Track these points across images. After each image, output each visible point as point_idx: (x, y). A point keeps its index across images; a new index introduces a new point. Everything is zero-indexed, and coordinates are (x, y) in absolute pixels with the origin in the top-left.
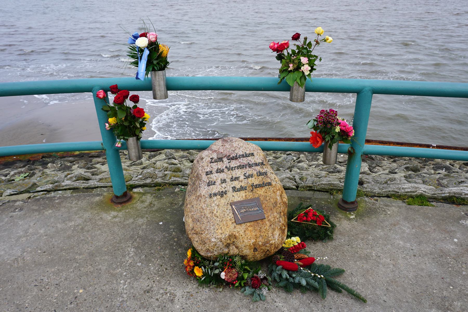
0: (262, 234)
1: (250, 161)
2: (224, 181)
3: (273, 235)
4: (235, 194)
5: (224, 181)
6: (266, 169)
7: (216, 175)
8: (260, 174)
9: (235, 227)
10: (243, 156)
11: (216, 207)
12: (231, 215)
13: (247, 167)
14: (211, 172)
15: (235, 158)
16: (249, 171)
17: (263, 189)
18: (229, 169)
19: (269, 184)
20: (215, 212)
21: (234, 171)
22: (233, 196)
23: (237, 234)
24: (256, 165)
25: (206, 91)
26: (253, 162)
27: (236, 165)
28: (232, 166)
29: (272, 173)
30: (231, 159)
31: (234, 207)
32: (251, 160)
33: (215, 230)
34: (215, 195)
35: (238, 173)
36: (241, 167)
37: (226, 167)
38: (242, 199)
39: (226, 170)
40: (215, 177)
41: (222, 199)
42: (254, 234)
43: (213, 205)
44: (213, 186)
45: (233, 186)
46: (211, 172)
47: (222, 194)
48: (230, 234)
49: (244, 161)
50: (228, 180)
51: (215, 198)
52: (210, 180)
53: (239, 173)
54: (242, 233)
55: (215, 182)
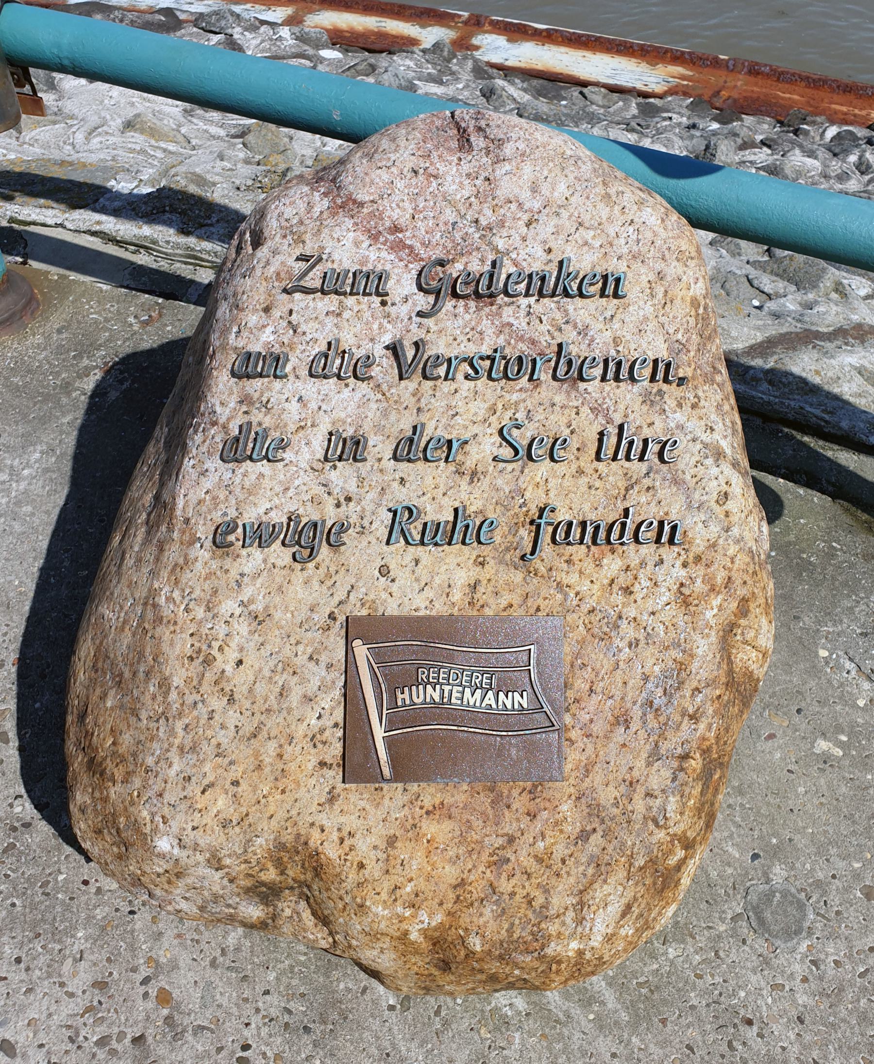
0: (505, 886)
1: (583, 332)
2: (349, 448)
3: (581, 903)
4: (399, 556)
5: (349, 448)
6: (679, 417)
7: (311, 388)
8: (619, 445)
9: (332, 798)
10: (539, 286)
11: (242, 628)
12: (331, 703)
13: (544, 375)
14: (278, 360)
15: (483, 291)
16: (547, 408)
17: (612, 565)
18: (413, 362)
19: (667, 534)
20: (225, 662)
21: (446, 387)
22: (384, 570)
23: (332, 852)
24: (617, 370)
25: (327, 139)
26: (601, 344)
27: (470, 349)
28: (438, 347)
29: (719, 455)
30: (440, 286)
31: (361, 650)
32: (591, 326)
33: (194, 789)
34: (261, 535)
35: (465, 409)
36: (505, 367)
37: (394, 349)
38: (440, 608)
39: (384, 368)
40: (294, 406)
41: (298, 577)
42: (450, 873)
43: (228, 606)
44: (263, 467)
45: (401, 496)
46: (278, 360)
47: (308, 539)
48: (288, 838)
49: (530, 323)
50: (380, 447)
51: (252, 559)
52: (257, 416)
53: (479, 408)
54: (365, 847)
55: (283, 445)
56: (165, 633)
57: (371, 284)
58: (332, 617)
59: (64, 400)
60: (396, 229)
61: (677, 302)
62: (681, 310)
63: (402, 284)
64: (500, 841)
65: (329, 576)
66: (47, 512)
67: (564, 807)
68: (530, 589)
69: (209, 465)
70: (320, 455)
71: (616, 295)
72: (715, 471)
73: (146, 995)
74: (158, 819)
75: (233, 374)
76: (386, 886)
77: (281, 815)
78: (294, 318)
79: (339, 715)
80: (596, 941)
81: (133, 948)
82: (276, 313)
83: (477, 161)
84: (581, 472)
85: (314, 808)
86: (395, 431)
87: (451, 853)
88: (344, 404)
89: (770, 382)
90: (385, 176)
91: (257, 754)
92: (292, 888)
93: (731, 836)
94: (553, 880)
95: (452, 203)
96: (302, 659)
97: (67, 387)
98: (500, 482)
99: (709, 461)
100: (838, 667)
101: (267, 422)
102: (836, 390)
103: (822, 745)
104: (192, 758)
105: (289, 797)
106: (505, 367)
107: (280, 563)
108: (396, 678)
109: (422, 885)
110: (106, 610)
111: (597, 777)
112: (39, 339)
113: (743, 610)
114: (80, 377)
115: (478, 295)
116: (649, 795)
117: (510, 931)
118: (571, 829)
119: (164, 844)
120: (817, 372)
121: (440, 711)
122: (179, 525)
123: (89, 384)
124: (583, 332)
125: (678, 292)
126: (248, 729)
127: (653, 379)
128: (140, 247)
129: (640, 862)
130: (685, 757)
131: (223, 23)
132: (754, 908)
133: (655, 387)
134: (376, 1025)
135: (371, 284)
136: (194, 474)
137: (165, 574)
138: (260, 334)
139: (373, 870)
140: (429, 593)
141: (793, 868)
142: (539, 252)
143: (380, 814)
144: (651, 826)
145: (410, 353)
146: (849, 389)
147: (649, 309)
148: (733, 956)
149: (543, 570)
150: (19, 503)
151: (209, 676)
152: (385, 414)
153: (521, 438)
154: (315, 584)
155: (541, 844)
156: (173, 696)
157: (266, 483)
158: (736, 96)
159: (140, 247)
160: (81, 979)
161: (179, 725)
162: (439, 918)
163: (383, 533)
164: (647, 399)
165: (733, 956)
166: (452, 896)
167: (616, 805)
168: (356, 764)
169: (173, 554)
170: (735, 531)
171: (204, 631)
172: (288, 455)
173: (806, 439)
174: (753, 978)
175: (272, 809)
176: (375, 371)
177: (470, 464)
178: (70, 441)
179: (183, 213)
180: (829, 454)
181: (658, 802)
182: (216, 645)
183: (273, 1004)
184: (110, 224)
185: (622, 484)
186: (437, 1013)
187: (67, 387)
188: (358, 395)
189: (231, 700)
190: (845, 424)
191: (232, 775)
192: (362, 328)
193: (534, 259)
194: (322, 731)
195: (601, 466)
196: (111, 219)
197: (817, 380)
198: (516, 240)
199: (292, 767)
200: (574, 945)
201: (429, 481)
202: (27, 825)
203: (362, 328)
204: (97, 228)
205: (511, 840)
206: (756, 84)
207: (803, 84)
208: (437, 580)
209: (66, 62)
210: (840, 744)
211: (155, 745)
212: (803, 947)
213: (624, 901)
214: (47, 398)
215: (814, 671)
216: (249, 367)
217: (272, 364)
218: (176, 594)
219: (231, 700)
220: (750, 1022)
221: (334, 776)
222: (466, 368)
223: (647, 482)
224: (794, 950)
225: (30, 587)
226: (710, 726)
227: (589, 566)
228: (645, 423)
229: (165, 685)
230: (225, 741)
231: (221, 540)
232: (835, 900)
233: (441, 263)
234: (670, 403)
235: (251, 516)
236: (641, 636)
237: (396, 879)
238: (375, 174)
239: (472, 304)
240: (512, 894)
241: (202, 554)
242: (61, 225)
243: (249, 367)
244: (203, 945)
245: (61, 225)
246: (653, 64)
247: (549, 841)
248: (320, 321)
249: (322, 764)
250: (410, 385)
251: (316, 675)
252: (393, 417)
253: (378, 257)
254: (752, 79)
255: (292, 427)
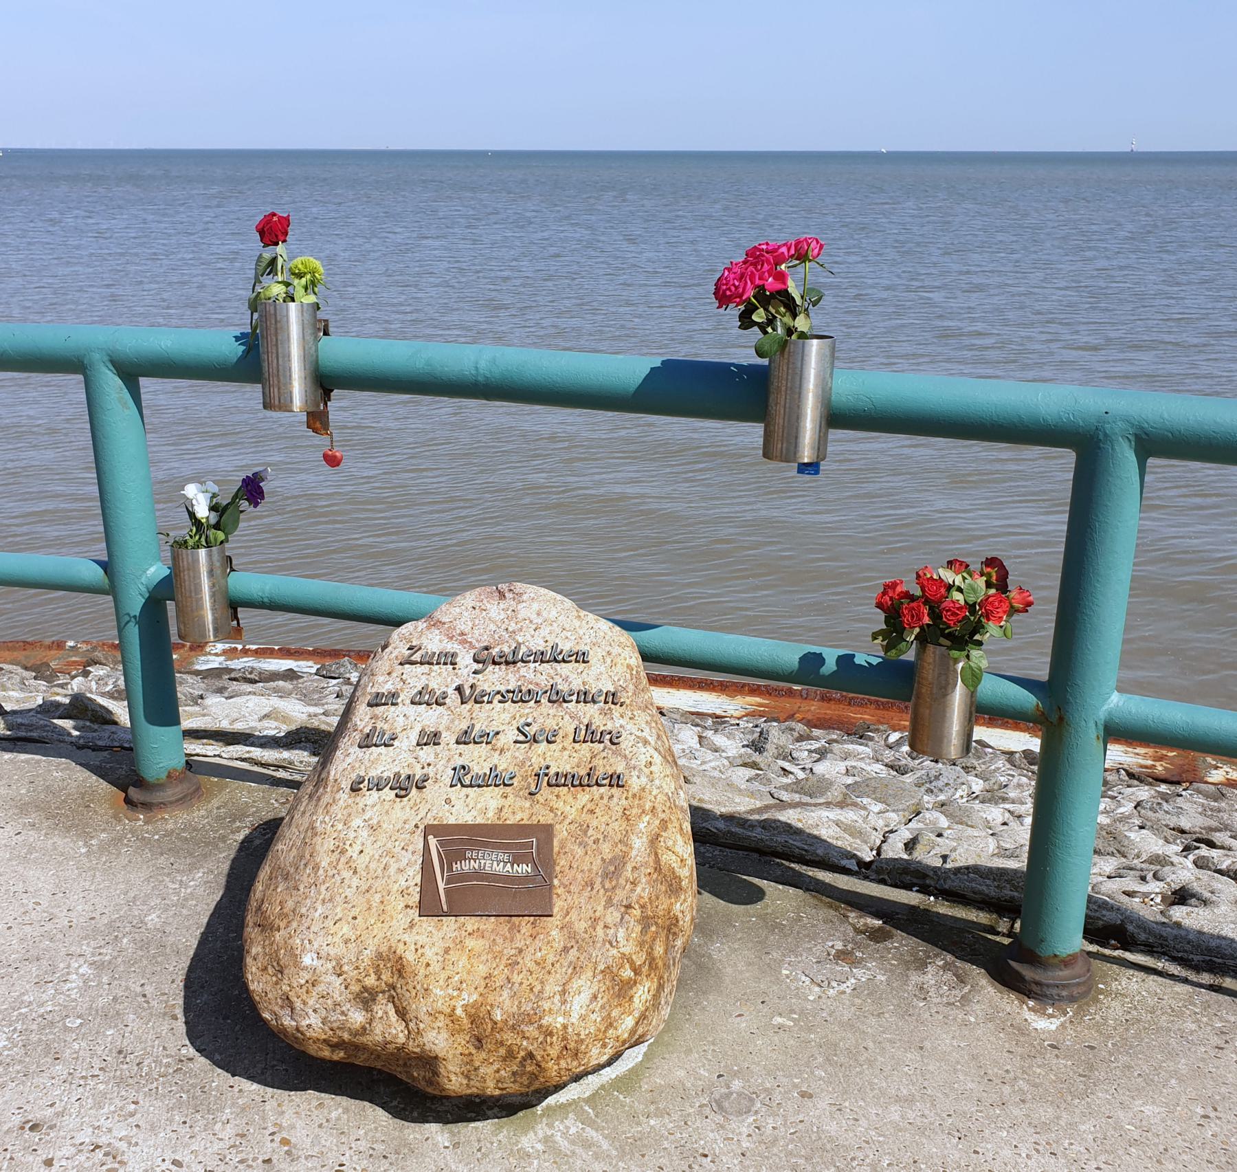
0: (516, 978)
1: (566, 679)
2: (431, 739)
3: (564, 992)
4: (458, 793)
5: (431, 739)
7: (412, 710)
9: (412, 925)
10: (541, 658)
11: (365, 833)
13: (544, 701)
14: (394, 695)
15: (509, 661)
16: (544, 716)
18: (469, 696)
19: (616, 781)
20: (353, 852)
22: (448, 801)
23: (410, 956)
24: (585, 697)
26: (577, 685)
29: (646, 742)
30: (484, 659)
31: (433, 841)
32: (570, 677)
36: (520, 696)
38: (479, 821)
39: (453, 698)
42: (482, 970)
43: (357, 822)
44: (382, 749)
45: (459, 762)
47: (403, 786)
48: (384, 949)
50: (448, 738)
52: (379, 725)
53: (506, 717)
56: (318, 840)
57: (450, 660)
58: (416, 826)
59: (221, 845)
60: (462, 634)
61: (619, 665)
62: (620, 669)
63: (465, 660)
64: (513, 952)
65: (415, 804)
66: (208, 904)
67: (553, 933)
68: (535, 810)
69: (351, 750)
70: (415, 743)
71: (584, 662)
72: (644, 750)
73: (272, 1141)
74: (306, 942)
75: (360, 747)
76: (443, 976)
77: (381, 935)
78: (404, 677)
79: (418, 879)
80: (574, 1019)
81: (264, 1119)
82: (394, 675)
83: (509, 602)
84: (564, 749)
85: (401, 931)
86: (457, 729)
87: (484, 958)
88: (430, 717)
89: (763, 828)
90: (458, 610)
91: (368, 901)
92: (383, 992)
93: (704, 1066)
94: (546, 977)
95: (494, 622)
96: (398, 849)
97: (223, 839)
98: (517, 754)
99: (640, 745)
100: (797, 979)
101: (386, 727)
102: (816, 833)
103: (778, 1020)
104: (330, 905)
105: (386, 925)
106: (520, 696)
107: (388, 799)
108: (452, 854)
109: (465, 976)
110: (280, 847)
111: (574, 915)
112: (203, 812)
113: (664, 824)
114: (233, 832)
115: (507, 663)
116: (606, 926)
117: (519, 1008)
118: (558, 946)
119: (307, 960)
120: (799, 820)
121: (478, 875)
122: (330, 783)
123: (241, 836)
124: (566, 679)
125: (619, 661)
126: (364, 888)
127: (606, 702)
128: (278, 767)
129: (601, 967)
130: (628, 907)
131: (342, 670)
132: (716, 1101)
133: (607, 706)
134: (434, 1155)
135: (450, 660)
136: (342, 757)
137: (320, 811)
138: (385, 685)
139: (435, 967)
140: (474, 813)
141: (748, 1081)
142: (542, 642)
143: (440, 935)
144: (608, 945)
145: (468, 692)
146: (827, 833)
147: (603, 669)
148: (698, 1124)
149: (542, 801)
150: (186, 899)
151: (343, 860)
152: (452, 721)
153: (531, 731)
154: (408, 809)
155: (539, 954)
156: (321, 872)
157: (383, 757)
158: (810, 717)
159: (278, 767)
160: (230, 1131)
161: (323, 888)
162: (475, 997)
163: (448, 782)
164: (603, 712)
165: (698, 1124)
166: (483, 984)
167: (586, 932)
168: (428, 906)
169: (326, 799)
170: (657, 782)
171: (342, 836)
172: (396, 743)
173: (792, 865)
174: (711, 1135)
175: (375, 932)
176: (447, 701)
177: (499, 745)
178: (226, 867)
179: (315, 742)
180: (810, 873)
181: (612, 931)
182: (348, 843)
183: (363, 1145)
184: (256, 753)
185: (589, 755)
186: (479, 1150)
187: (223, 839)
188: (438, 712)
189: (355, 872)
190: (820, 852)
191: (352, 914)
192: (440, 679)
193: (537, 644)
194: (407, 888)
195: (577, 746)
196: (259, 749)
197: (800, 825)
198: (528, 637)
199: (389, 908)
200: (561, 1020)
201: (476, 754)
202: (191, 1059)
203: (440, 679)
204: (247, 756)
205: (521, 951)
206: (829, 709)
207: (873, 706)
208: (479, 806)
209: (266, 600)
210: (793, 1020)
211: (308, 901)
212: (751, 1119)
213: (592, 991)
214: (207, 844)
215: (778, 981)
216: (376, 702)
217: (391, 699)
218: (327, 819)
219: (355, 872)
220: (706, 1156)
221: (414, 913)
222: (499, 697)
223: (604, 754)
224: (743, 1121)
225: (194, 943)
226: (644, 889)
227: (570, 799)
228: (599, 723)
229: (316, 868)
230: (349, 895)
231: (355, 789)
232: (777, 1098)
233: (487, 648)
234: (616, 714)
235: (373, 773)
236: (601, 837)
237: (448, 973)
238: (452, 610)
239: (503, 667)
240: (521, 984)
241: (344, 797)
242: (219, 756)
243: (376, 702)
244: (314, 1117)
245: (219, 756)
246: (732, 696)
247: (544, 952)
248: (417, 677)
249: (407, 906)
250: (467, 706)
251: (406, 857)
252: (457, 722)
253: (451, 647)
254: (825, 704)
255: (399, 730)
